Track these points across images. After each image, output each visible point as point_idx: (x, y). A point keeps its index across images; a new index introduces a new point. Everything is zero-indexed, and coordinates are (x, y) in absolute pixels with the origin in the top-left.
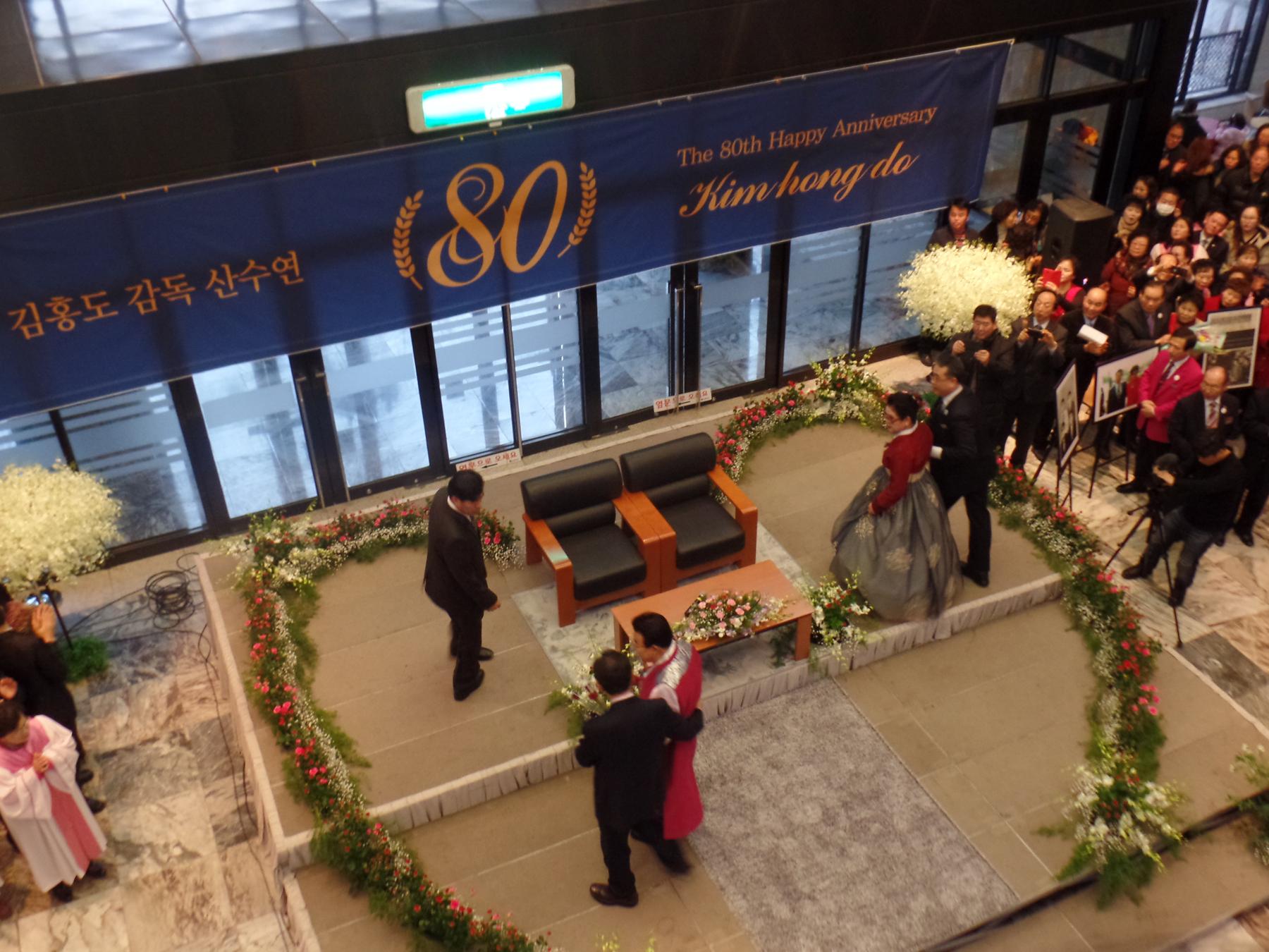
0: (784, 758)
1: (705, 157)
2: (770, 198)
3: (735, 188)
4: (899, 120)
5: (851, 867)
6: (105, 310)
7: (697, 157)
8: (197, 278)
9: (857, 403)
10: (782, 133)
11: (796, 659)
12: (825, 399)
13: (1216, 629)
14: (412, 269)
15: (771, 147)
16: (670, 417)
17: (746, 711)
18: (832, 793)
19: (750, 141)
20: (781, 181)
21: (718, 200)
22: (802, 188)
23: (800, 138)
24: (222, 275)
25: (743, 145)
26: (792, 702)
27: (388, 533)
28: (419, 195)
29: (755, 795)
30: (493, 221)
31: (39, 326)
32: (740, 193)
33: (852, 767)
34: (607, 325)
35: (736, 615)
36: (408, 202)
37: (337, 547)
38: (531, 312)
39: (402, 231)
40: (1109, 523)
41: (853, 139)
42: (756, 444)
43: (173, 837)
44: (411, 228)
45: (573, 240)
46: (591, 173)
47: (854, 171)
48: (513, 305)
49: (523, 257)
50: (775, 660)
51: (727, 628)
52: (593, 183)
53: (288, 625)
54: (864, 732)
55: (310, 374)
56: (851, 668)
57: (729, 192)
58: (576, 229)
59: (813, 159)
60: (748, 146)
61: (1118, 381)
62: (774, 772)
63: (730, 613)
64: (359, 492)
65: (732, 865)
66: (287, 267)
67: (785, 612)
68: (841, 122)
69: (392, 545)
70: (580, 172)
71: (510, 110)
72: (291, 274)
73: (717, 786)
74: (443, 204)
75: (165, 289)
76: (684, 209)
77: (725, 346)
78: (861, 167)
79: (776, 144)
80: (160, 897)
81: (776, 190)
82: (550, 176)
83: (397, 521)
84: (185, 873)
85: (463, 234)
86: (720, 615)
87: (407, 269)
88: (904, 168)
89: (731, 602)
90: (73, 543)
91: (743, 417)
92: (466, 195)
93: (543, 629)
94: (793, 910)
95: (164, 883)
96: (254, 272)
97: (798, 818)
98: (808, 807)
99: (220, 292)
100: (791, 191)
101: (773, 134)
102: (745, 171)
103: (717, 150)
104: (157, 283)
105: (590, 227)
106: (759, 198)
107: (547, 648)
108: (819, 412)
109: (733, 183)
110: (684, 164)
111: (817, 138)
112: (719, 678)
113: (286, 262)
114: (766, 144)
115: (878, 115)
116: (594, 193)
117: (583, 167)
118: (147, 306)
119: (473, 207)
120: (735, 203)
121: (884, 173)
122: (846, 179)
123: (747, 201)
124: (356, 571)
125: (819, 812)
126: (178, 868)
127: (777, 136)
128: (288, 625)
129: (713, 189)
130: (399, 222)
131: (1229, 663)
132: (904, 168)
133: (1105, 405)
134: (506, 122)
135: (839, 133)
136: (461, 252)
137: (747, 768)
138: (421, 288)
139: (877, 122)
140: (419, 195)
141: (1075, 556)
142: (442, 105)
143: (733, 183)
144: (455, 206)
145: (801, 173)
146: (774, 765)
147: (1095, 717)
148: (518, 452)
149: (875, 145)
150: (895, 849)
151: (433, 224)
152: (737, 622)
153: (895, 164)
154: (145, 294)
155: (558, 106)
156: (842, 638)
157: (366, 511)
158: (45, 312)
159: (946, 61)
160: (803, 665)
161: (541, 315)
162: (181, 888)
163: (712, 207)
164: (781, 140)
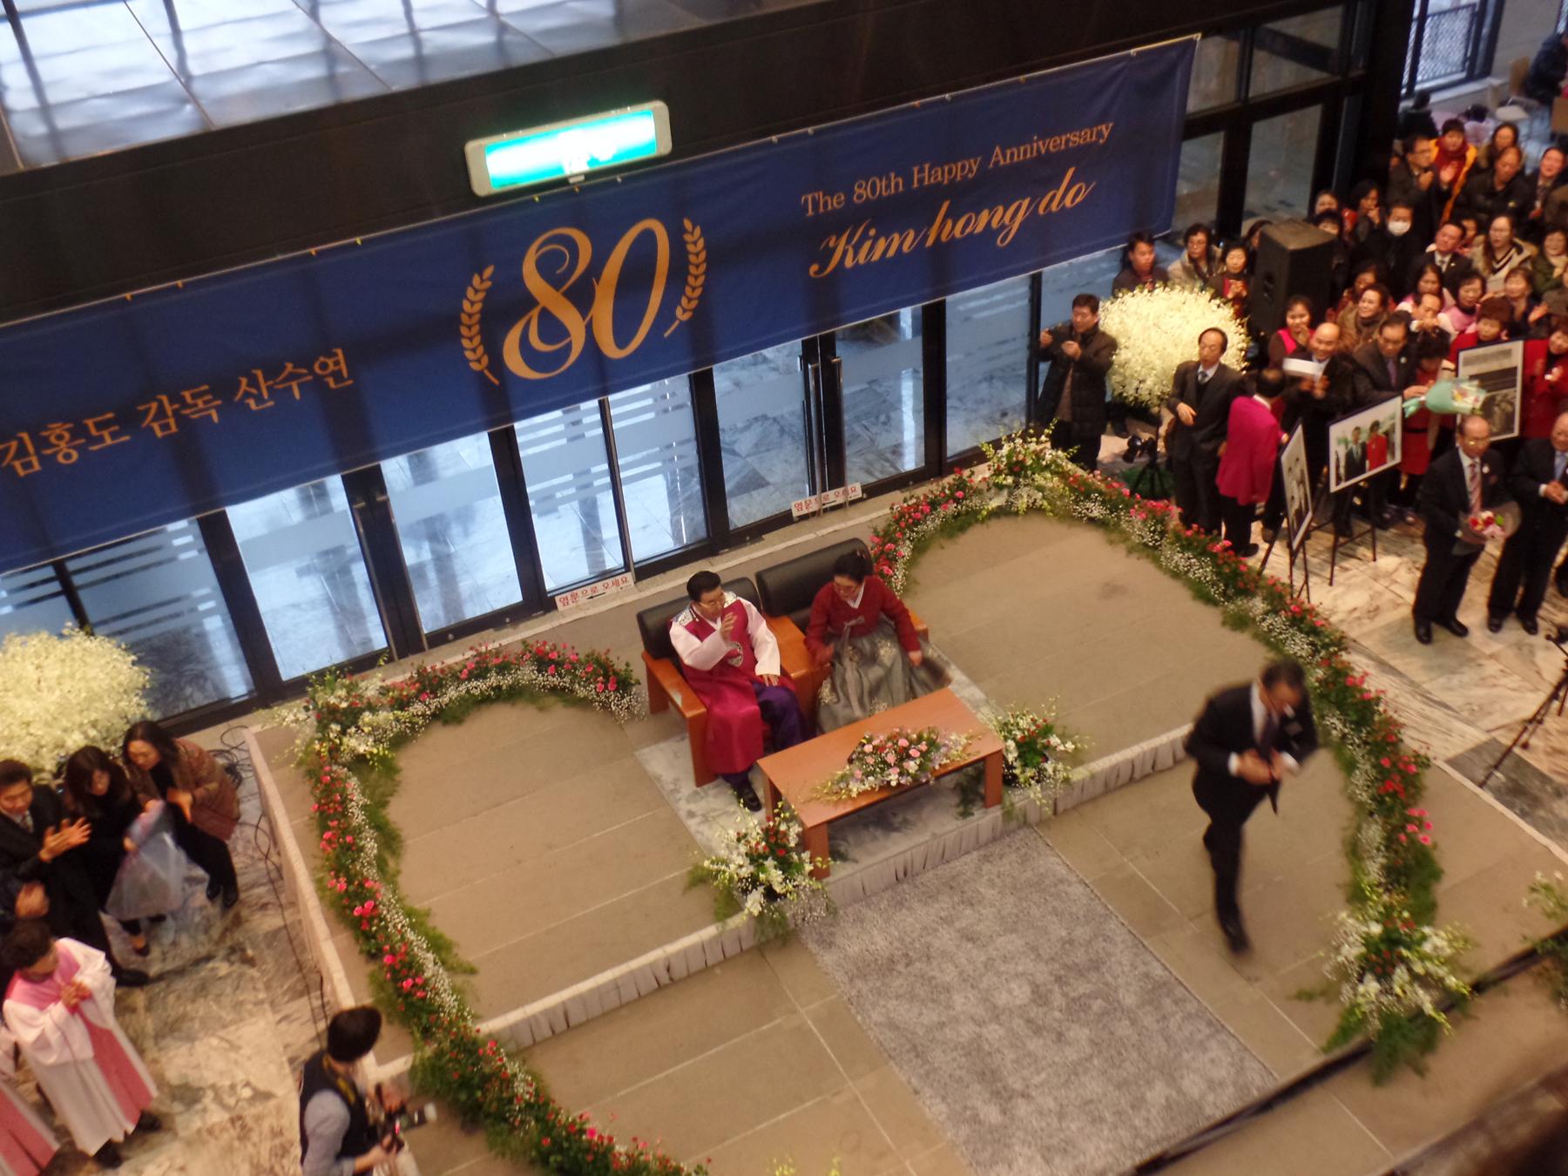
0: (981, 927)
1: (835, 202)
2: (919, 247)
3: (876, 239)
4: (1067, 141)
5: (1071, 1054)
6: (114, 435)
7: (826, 204)
8: (223, 389)
9: (1040, 489)
10: (927, 166)
11: (986, 806)
12: (1000, 487)
13: (1495, 734)
14: (485, 360)
15: (916, 185)
16: (813, 521)
17: (930, 874)
18: (1042, 967)
19: (889, 179)
20: (930, 225)
21: (856, 254)
22: (957, 233)
23: (950, 172)
24: (253, 382)
25: (881, 185)
26: (986, 858)
27: (478, 687)
28: (489, 271)
29: (949, 975)
30: (582, 297)
31: (35, 460)
32: (882, 243)
33: (1064, 933)
34: (728, 414)
35: (909, 757)
36: (476, 280)
37: (418, 708)
38: (635, 406)
39: (470, 316)
40: (1356, 614)
41: (1015, 168)
42: (920, 548)
43: (240, 1077)
44: (482, 311)
45: (682, 315)
46: (698, 231)
47: (1019, 207)
48: (612, 398)
49: (622, 339)
50: (961, 809)
51: (901, 774)
52: (701, 243)
53: (364, 807)
54: (1077, 890)
55: (370, 499)
56: (1055, 812)
57: (868, 244)
58: (684, 301)
59: (967, 197)
60: (888, 186)
61: (1356, 441)
62: (970, 945)
63: (903, 755)
64: (439, 638)
65: (926, 1062)
66: (332, 367)
67: (969, 750)
68: (998, 149)
69: (484, 700)
70: (685, 231)
71: (593, 161)
72: (337, 376)
73: (900, 967)
74: (519, 279)
75: (185, 405)
76: (814, 268)
77: (874, 430)
78: (1026, 202)
79: (921, 181)
80: (229, 1150)
81: (926, 237)
82: (648, 237)
83: (488, 670)
84: (258, 1118)
85: (546, 315)
86: (891, 758)
87: (479, 361)
88: (1078, 200)
89: (903, 742)
90: (94, 725)
91: (902, 515)
92: (546, 266)
93: (676, 791)
94: (1004, 1112)
95: (233, 1133)
96: (292, 377)
97: (1002, 999)
98: (1013, 985)
99: (252, 403)
100: (944, 238)
101: (916, 170)
102: (885, 216)
103: (849, 192)
104: (175, 398)
105: (700, 298)
106: (905, 248)
107: (682, 814)
108: (994, 504)
109: (872, 232)
110: (810, 213)
111: (970, 170)
112: (895, 835)
113: (330, 362)
114: (908, 181)
115: (1042, 137)
116: (703, 256)
117: (687, 224)
118: (165, 427)
119: (556, 283)
120: (876, 256)
121: (1054, 207)
122: (1009, 218)
123: (891, 253)
124: (441, 736)
125: (1027, 989)
126: (250, 1112)
127: (921, 171)
128: (364, 807)
129: (848, 242)
130: (466, 305)
131: (1513, 776)
132: (1078, 200)
133: (1342, 471)
134: (589, 176)
135: (997, 162)
136: (544, 338)
137: (937, 943)
138: (496, 382)
139: (1040, 146)
140: (489, 271)
141: (1317, 658)
142: (510, 160)
143: (872, 232)
144: (534, 281)
145: (953, 215)
146: (969, 937)
147: (1354, 851)
148: (630, 576)
149: (1039, 176)
150: (1123, 1029)
151: (508, 305)
152: (912, 766)
153: (1067, 195)
154: (161, 413)
155: (653, 153)
156: (1040, 777)
157: (450, 661)
158: (41, 443)
159: (1120, 66)
160: (995, 813)
161: (648, 409)
162: (255, 1137)
163: (849, 263)
164: (927, 175)
